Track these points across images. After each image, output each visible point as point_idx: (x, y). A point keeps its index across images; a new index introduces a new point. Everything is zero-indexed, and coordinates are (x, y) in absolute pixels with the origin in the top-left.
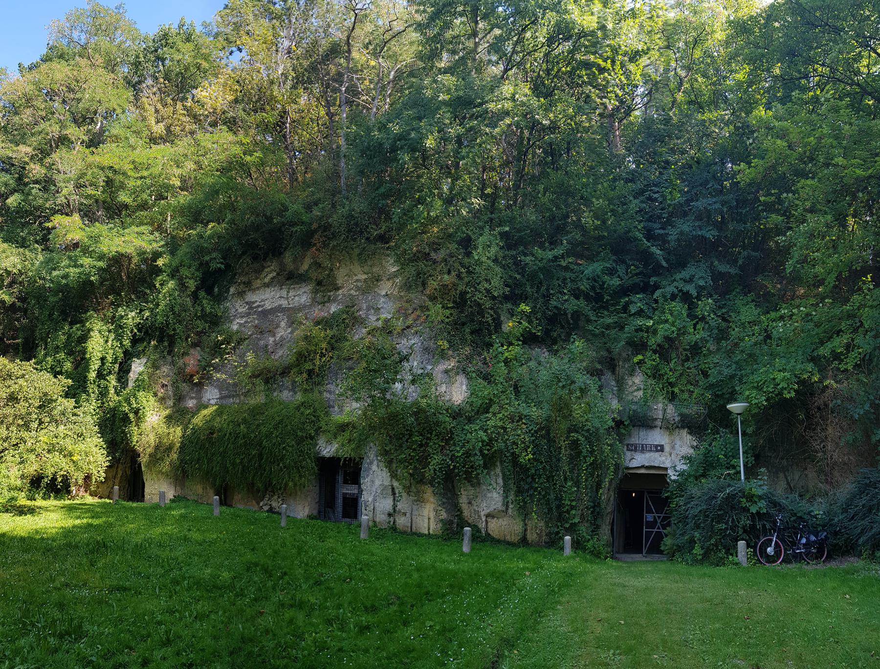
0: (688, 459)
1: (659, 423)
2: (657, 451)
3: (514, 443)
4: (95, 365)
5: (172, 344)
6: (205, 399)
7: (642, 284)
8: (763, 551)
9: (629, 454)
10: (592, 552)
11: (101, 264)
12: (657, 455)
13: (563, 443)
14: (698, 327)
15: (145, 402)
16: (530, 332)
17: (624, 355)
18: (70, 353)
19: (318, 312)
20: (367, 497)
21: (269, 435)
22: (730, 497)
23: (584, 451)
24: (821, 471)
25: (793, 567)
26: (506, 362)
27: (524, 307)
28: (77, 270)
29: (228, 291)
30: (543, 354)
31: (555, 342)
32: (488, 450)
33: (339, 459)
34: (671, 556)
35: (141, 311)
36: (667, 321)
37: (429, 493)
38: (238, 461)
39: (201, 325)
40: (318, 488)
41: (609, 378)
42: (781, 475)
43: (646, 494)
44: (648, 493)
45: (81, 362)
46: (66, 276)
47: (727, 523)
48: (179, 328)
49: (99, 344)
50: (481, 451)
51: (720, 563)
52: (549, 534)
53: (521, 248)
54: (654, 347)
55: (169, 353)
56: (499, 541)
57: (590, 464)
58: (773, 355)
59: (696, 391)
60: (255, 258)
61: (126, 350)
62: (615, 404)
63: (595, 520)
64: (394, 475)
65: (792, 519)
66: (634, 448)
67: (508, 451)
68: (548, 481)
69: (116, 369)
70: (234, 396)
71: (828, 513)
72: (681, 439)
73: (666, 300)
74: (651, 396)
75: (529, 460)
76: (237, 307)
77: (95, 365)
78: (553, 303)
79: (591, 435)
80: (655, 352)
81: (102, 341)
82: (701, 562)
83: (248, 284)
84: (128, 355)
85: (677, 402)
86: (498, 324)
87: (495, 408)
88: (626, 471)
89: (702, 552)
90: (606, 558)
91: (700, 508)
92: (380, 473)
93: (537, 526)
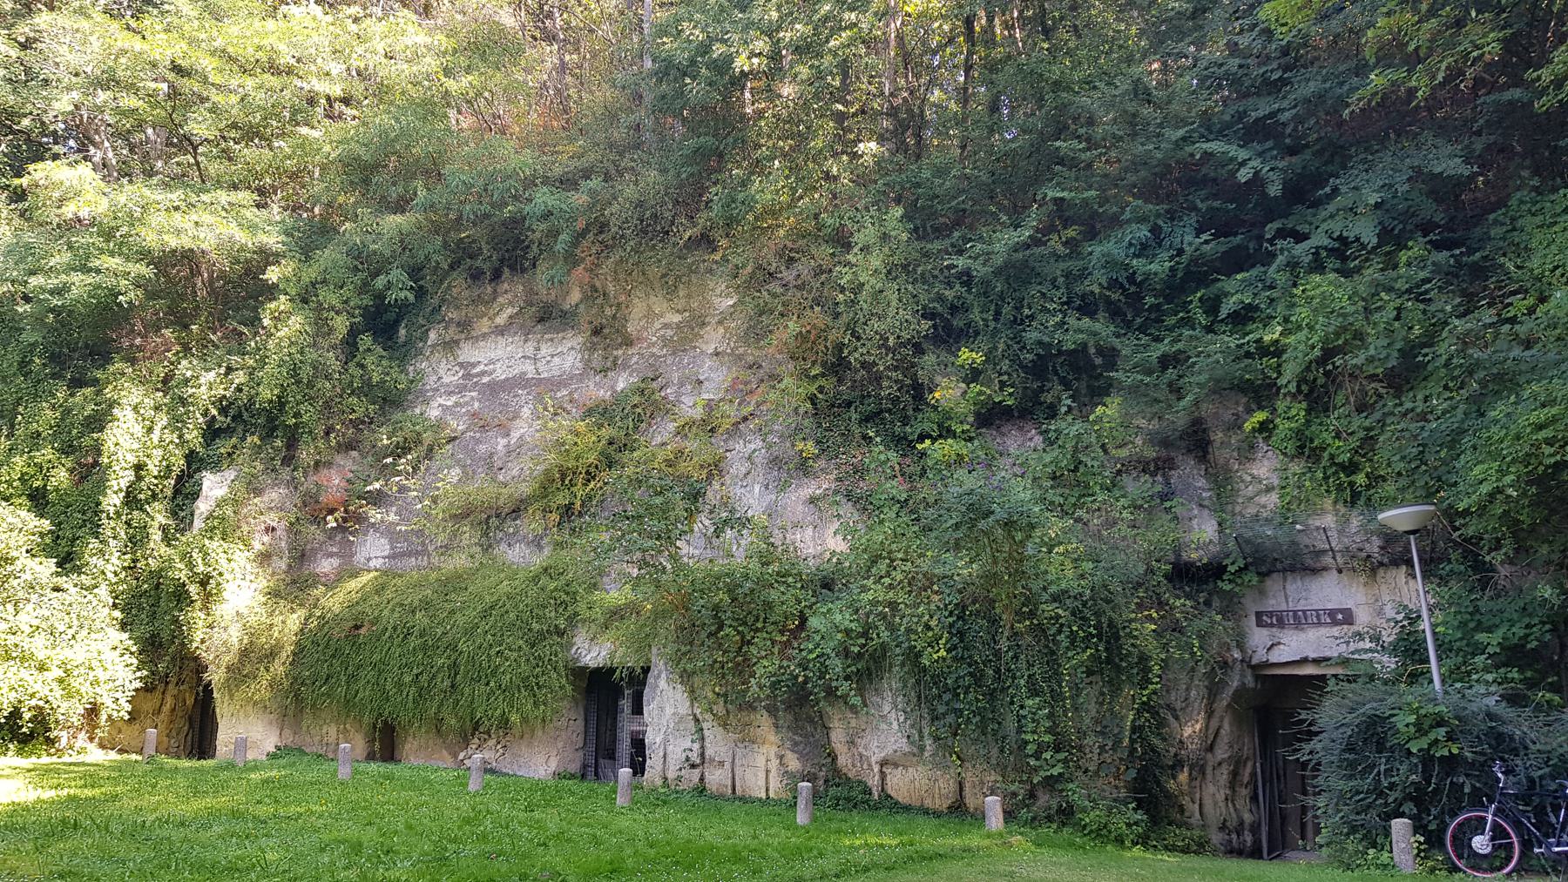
2: (1335, 623)
4: (120, 479)
5: (292, 444)
6: (360, 558)
11: (142, 269)
15: (223, 562)
18: (67, 449)
19: (597, 391)
20: (653, 738)
21: (470, 632)
28: (90, 279)
29: (424, 337)
33: (612, 670)
35: (229, 370)
38: (407, 679)
39: (361, 407)
40: (581, 723)
41: (1189, 473)
45: (90, 471)
46: (59, 291)
48: (308, 413)
49: (134, 435)
55: (288, 460)
56: (907, 809)
60: (476, 276)
61: (192, 452)
64: (693, 696)
66: (1279, 621)
69: (169, 492)
70: (417, 553)
76: (442, 373)
77: (120, 479)
81: (138, 430)
83: (465, 326)
84: (195, 463)
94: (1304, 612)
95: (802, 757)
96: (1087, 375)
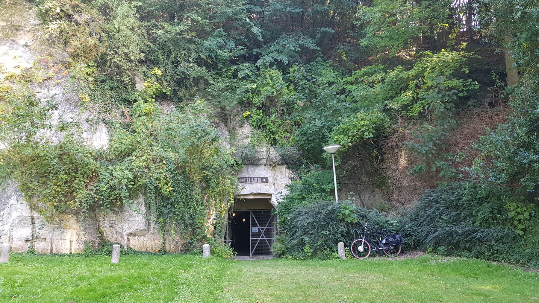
2: (263, 182)
8: (355, 249)
13: (196, 178)
14: (290, 88)
17: (235, 111)
22: (332, 212)
25: (377, 259)
27: (158, 71)
31: (180, 100)
32: (133, 185)
36: (268, 84)
37: (71, 220)
43: (251, 213)
44: (253, 212)
47: (329, 231)
50: (126, 186)
51: (326, 257)
52: (184, 245)
53: (153, 21)
56: (141, 253)
64: (33, 207)
66: (245, 181)
68: (184, 206)
71: (400, 222)
73: (266, 68)
78: (181, 69)
80: (259, 108)
82: (311, 257)
85: (278, 146)
89: (312, 251)
92: (19, 206)
93: (174, 239)
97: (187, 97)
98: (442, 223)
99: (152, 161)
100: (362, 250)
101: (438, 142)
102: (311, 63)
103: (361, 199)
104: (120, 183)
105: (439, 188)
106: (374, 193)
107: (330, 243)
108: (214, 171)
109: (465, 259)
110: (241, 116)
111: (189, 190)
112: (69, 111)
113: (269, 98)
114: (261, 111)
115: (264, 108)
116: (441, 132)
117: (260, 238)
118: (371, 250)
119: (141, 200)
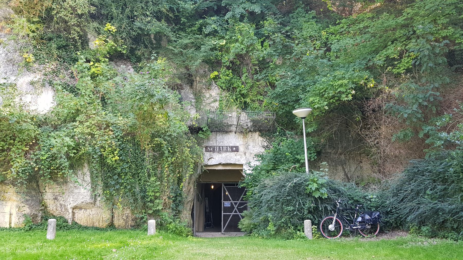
0: (260, 156)
1: (233, 128)
2: (232, 151)
3: (102, 147)
7: (216, 8)
8: (325, 228)
9: (207, 155)
10: (174, 232)
12: (233, 154)
14: (265, 44)
16: (116, 50)
22: (297, 186)
23: (166, 152)
24: (374, 164)
25: (351, 240)
26: (93, 77)
30: (126, 70)
31: (139, 60)
32: (74, 153)
34: (249, 232)
36: (237, 41)
41: (187, 92)
42: (340, 168)
43: (223, 185)
44: (225, 185)
47: (294, 206)
51: (290, 237)
52: (135, 220)
54: (228, 64)
56: (86, 228)
57: (172, 163)
58: (333, 67)
59: (265, 100)
62: (193, 114)
63: (177, 206)
65: (350, 202)
66: (213, 150)
67: (96, 153)
72: (254, 140)
73: (236, 22)
74: (226, 106)
75: (116, 161)
78: (137, 24)
79: (172, 139)
80: (228, 68)
85: (249, 110)
86: (85, 42)
87: (81, 117)
88: (205, 168)
89: (275, 229)
90: (187, 236)
91: (271, 195)
93: (123, 214)
94: (222, 147)
95: (30, 206)
96: (157, 44)
97: (146, 56)
98: (427, 199)
99: (102, 127)
100: (333, 229)
101: (425, 103)
102: (291, 15)
103: (345, 172)
104: (59, 152)
105: (427, 157)
106: (361, 165)
107: (295, 220)
108: (168, 139)
109: (452, 241)
110: (208, 78)
111: (140, 160)
112: (11, 72)
113: (239, 56)
114: (231, 71)
115: (235, 68)
116: (430, 92)
117: (233, 213)
118: (344, 229)
119: (86, 170)
